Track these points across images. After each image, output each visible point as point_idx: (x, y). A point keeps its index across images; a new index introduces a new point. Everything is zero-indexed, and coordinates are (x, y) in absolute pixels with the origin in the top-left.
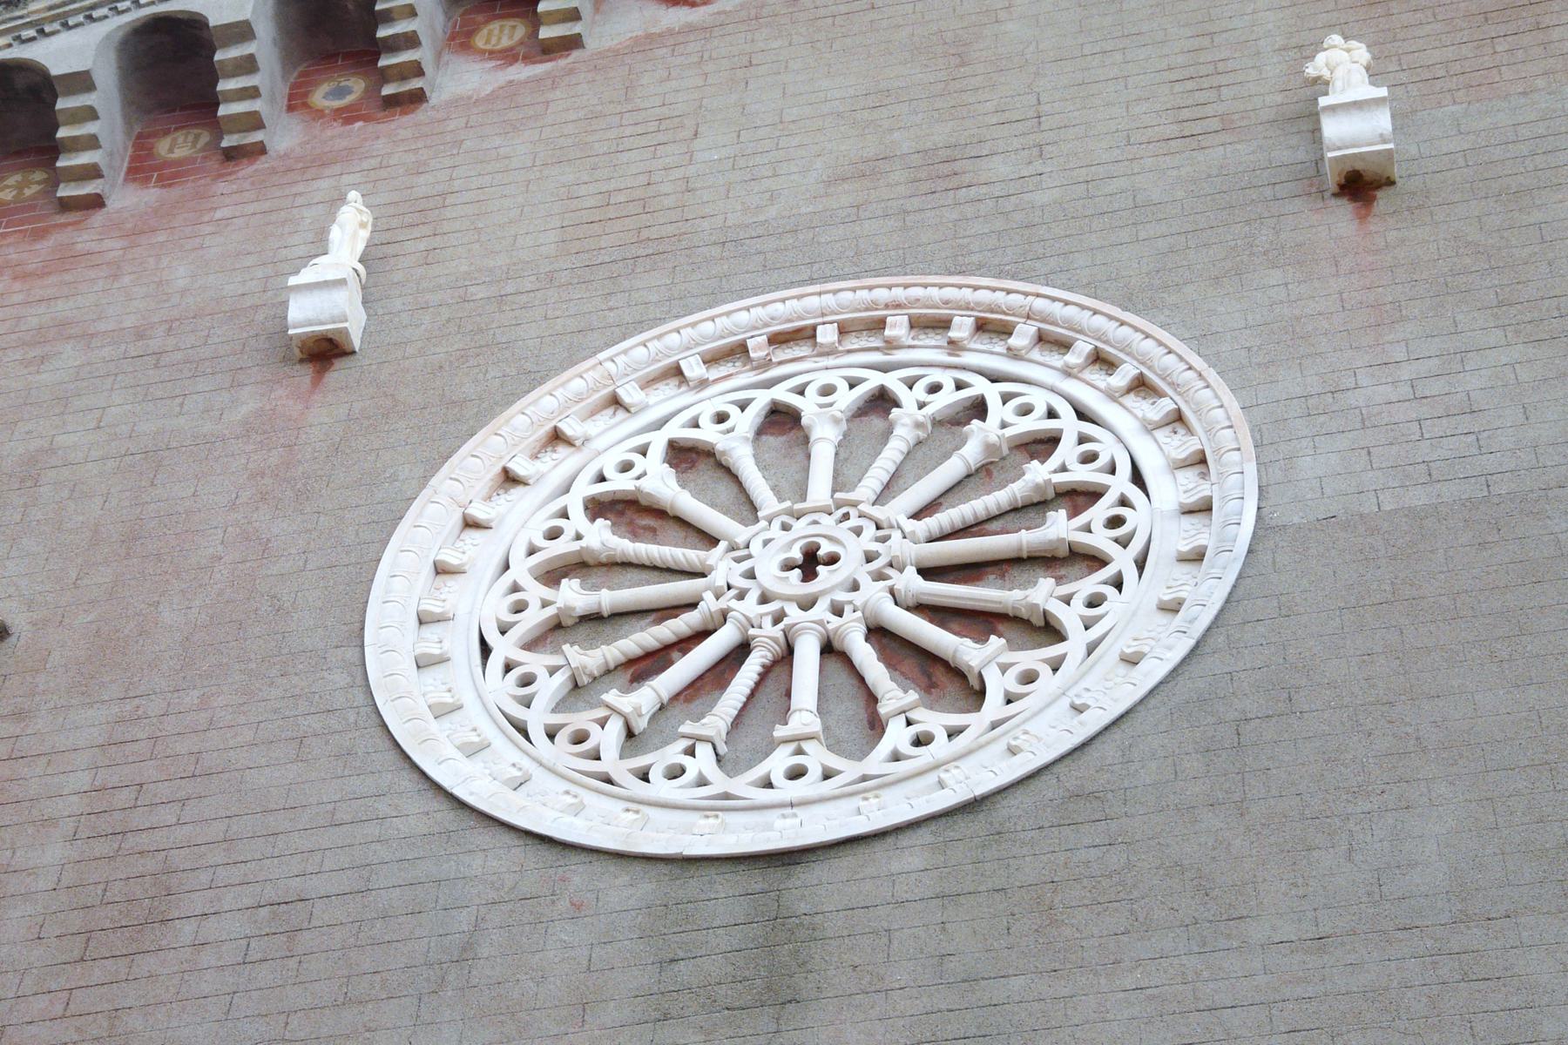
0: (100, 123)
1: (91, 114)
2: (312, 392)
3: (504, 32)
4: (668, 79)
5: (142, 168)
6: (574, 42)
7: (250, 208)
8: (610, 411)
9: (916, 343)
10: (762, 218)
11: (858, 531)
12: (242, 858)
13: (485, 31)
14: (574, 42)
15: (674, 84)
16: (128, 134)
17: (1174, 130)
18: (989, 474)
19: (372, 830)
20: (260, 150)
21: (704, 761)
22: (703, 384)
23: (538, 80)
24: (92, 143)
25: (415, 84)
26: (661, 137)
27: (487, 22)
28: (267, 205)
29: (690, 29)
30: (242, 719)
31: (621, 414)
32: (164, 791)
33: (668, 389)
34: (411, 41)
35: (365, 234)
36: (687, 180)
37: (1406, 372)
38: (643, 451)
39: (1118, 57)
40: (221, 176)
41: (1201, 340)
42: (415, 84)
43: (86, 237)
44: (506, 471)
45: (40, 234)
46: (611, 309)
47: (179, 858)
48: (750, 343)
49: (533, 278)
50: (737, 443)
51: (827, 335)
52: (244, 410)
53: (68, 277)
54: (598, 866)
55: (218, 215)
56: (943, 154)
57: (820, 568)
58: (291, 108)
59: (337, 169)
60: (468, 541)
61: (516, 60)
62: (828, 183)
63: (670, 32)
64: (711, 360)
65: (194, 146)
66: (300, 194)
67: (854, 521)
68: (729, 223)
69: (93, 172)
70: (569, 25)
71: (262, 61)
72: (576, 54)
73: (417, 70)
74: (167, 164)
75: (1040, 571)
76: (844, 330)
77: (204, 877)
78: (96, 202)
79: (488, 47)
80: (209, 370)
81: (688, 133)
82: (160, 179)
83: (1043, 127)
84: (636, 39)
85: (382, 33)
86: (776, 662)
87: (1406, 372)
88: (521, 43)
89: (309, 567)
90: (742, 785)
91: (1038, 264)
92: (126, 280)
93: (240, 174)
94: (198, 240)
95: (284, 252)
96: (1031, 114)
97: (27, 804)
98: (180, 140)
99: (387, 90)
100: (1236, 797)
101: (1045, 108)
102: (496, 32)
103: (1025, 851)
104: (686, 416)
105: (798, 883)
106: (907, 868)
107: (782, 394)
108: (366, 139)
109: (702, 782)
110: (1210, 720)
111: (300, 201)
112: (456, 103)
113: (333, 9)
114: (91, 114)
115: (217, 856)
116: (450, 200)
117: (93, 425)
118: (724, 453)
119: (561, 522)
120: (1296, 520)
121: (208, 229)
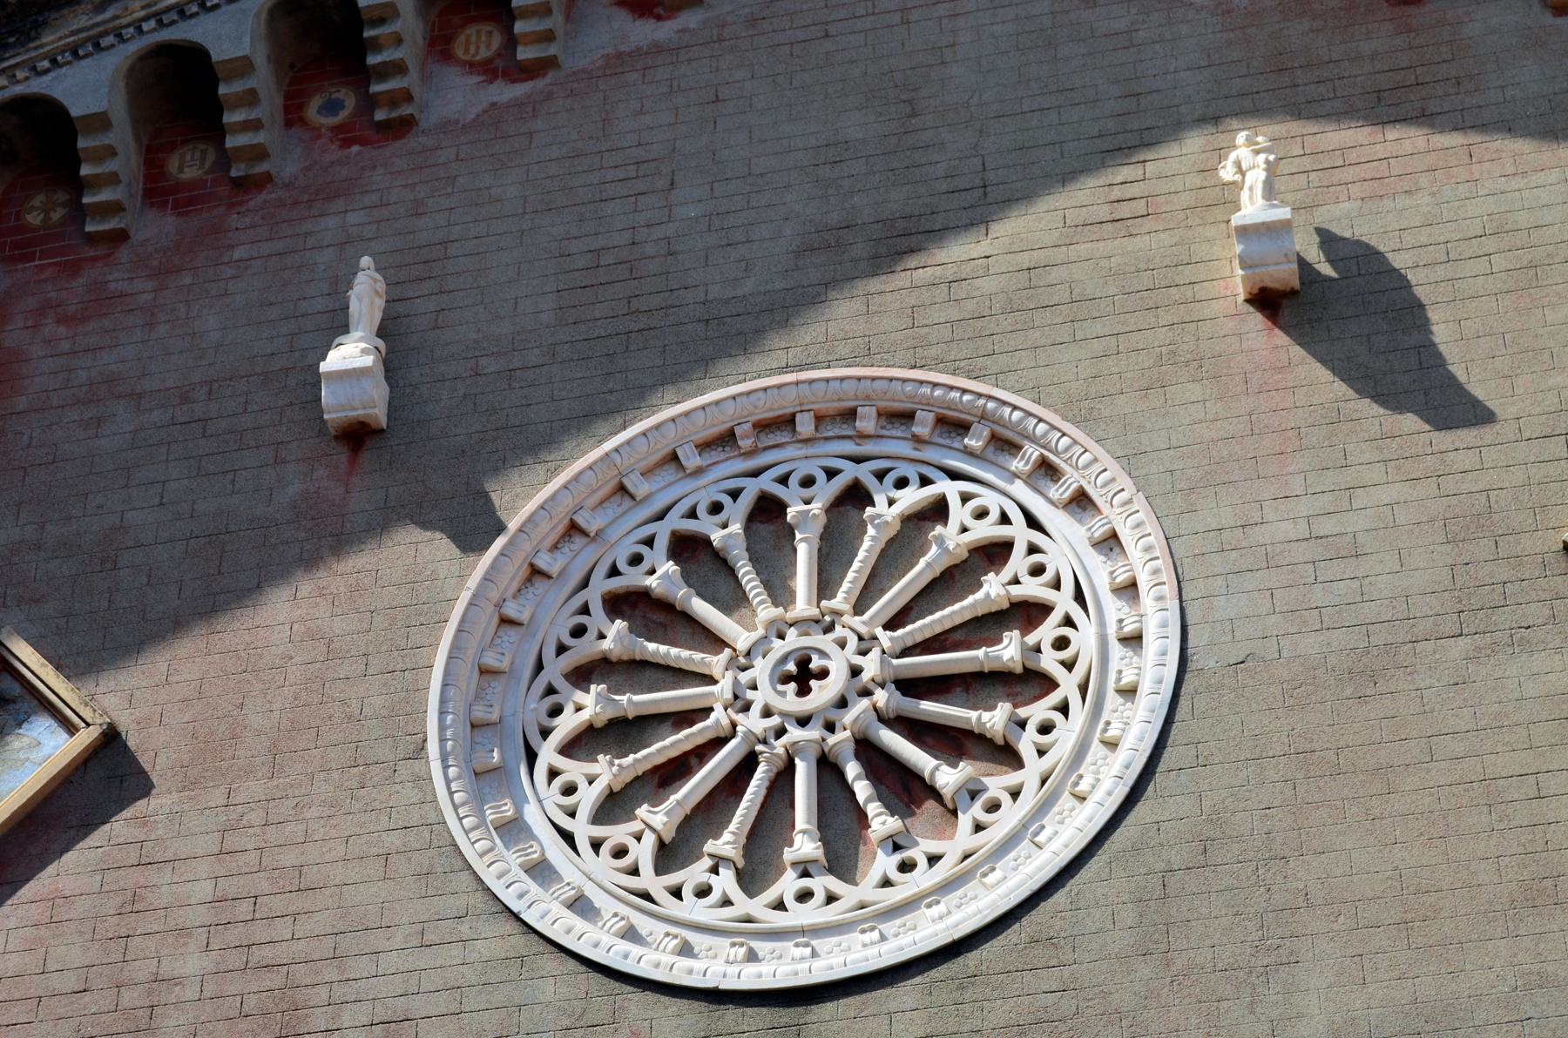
0: (113, 162)
1: (111, 152)
2: (350, 474)
3: (480, 41)
4: (641, 112)
5: (159, 190)
6: (549, 64)
7: (266, 248)
8: (617, 498)
9: (884, 432)
10: (740, 293)
11: (842, 644)
12: (352, 976)
13: (462, 38)
14: (549, 64)
15: (647, 119)
16: (137, 138)
17: (1103, 212)
18: (952, 577)
19: (456, 951)
20: (267, 179)
21: (725, 882)
22: (699, 471)
23: (518, 104)
24: (113, 179)
25: (406, 110)
26: (641, 185)
27: (463, 26)
28: (280, 246)
29: (658, 49)
30: (334, 833)
31: (627, 503)
32: (278, 904)
33: (669, 474)
34: (398, 68)
35: (380, 303)
36: (667, 239)
37: (1304, 507)
38: (649, 542)
39: (1053, 117)
40: (233, 205)
41: (1130, 460)
42: (406, 110)
43: (116, 275)
44: (532, 565)
45: (73, 269)
46: (611, 392)
47: (302, 974)
48: (738, 431)
49: (537, 351)
50: (727, 533)
51: (805, 425)
52: (292, 491)
53: (107, 323)
54: (650, 997)
55: (237, 255)
56: (900, 224)
57: (813, 683)
58: (289, 124)
59: (339, 204)
60: (505, 638)
61: (496, 77)
62: (798, 254)
63: (639, 52)
64: (705, 446)
65: (201, 166)
66: (307, 234)
67: (839, 631)
68: (710, 297)
69: (115, 208)
70: (544, 45)
71: (263, 94)
72: (551, 76)
73: (408, 97)
74: (180, 187)
75: (1001, 690)
76: (819, 419)
77: (323, 993)
78: (121, 236)
79: (468, 58)
80: (253, 443)
81: (662, 183)
82: (174, 207)
83: (990, 200)
84: (608, 57)
85: (373, 60)
86: (779, 775)
87: (1304, 507)
88: (498, 55)
89: (371, 671)
90: (757, 906)
91: (988, 361)
92: (162, 329)
93: (252, 203)
94: (222, 284)
95: (305, 304)
96: (978, 182)
97: (163, 913)
98: (188, 157)
99: (380, 115)
100: (1163, 947)
101: (991, 176)
102: (474, 39)
103: (996, 994)
104: (683, 507)
105: (815, 1018)
106: (902, 1007)
107: (766, 483)
108: (363, 168)
109: (727, 902)
110: (1143, 871)
111: (311, 242)
112: (445, 126)
113: (322, 30)
114: (111, 152)
115: (330, 973)
116: (452, 251)
117: (157, 501)
118: (722, 549)
119: (583, 619)
120: (1212, 664)
121: (229, 272)
